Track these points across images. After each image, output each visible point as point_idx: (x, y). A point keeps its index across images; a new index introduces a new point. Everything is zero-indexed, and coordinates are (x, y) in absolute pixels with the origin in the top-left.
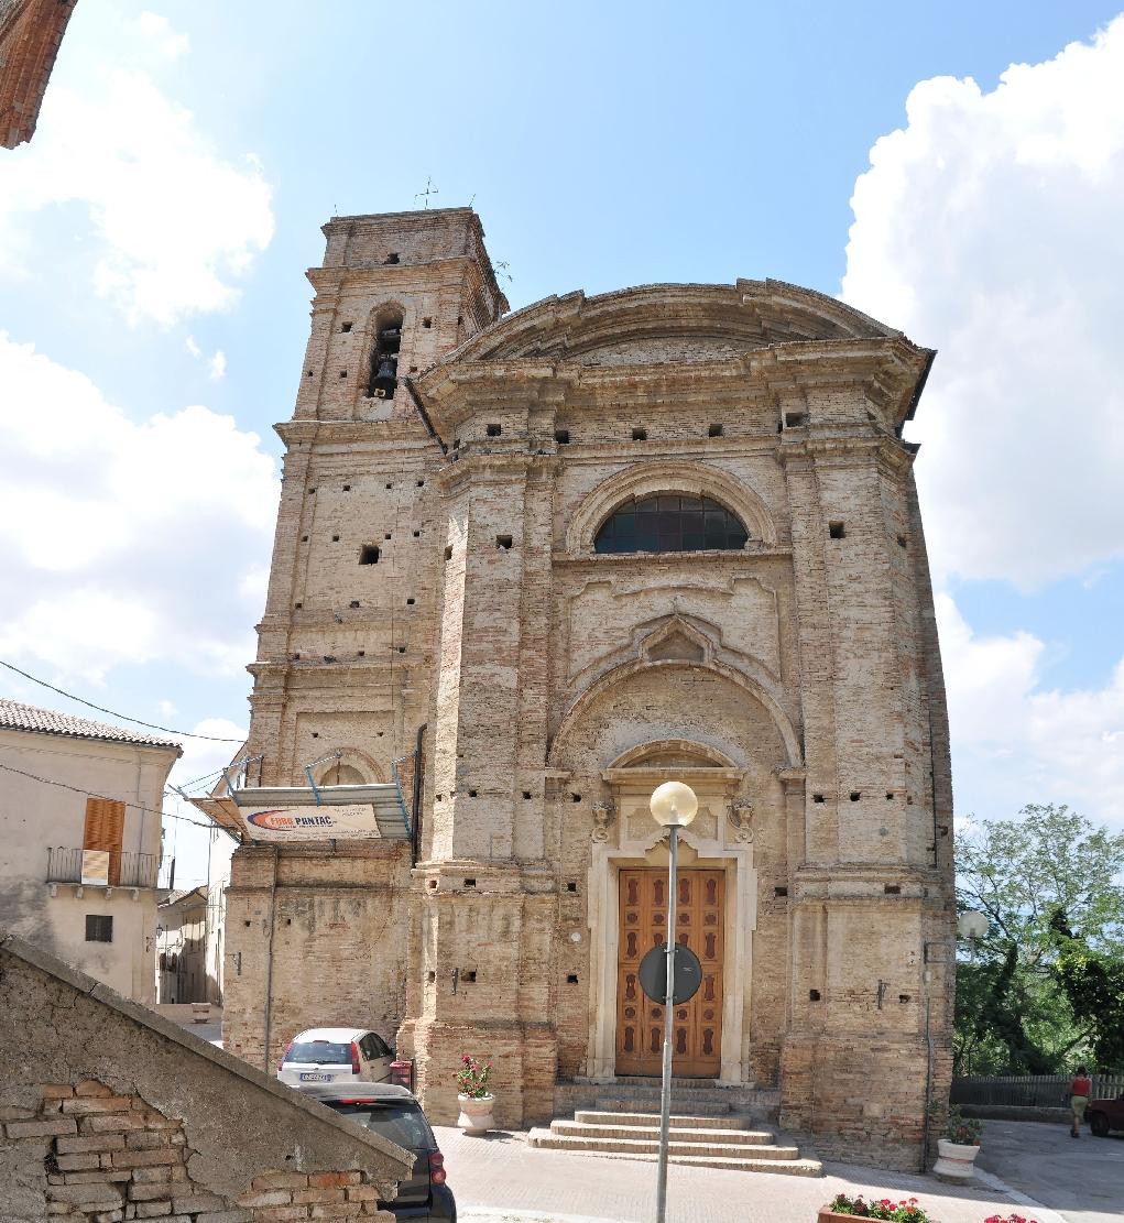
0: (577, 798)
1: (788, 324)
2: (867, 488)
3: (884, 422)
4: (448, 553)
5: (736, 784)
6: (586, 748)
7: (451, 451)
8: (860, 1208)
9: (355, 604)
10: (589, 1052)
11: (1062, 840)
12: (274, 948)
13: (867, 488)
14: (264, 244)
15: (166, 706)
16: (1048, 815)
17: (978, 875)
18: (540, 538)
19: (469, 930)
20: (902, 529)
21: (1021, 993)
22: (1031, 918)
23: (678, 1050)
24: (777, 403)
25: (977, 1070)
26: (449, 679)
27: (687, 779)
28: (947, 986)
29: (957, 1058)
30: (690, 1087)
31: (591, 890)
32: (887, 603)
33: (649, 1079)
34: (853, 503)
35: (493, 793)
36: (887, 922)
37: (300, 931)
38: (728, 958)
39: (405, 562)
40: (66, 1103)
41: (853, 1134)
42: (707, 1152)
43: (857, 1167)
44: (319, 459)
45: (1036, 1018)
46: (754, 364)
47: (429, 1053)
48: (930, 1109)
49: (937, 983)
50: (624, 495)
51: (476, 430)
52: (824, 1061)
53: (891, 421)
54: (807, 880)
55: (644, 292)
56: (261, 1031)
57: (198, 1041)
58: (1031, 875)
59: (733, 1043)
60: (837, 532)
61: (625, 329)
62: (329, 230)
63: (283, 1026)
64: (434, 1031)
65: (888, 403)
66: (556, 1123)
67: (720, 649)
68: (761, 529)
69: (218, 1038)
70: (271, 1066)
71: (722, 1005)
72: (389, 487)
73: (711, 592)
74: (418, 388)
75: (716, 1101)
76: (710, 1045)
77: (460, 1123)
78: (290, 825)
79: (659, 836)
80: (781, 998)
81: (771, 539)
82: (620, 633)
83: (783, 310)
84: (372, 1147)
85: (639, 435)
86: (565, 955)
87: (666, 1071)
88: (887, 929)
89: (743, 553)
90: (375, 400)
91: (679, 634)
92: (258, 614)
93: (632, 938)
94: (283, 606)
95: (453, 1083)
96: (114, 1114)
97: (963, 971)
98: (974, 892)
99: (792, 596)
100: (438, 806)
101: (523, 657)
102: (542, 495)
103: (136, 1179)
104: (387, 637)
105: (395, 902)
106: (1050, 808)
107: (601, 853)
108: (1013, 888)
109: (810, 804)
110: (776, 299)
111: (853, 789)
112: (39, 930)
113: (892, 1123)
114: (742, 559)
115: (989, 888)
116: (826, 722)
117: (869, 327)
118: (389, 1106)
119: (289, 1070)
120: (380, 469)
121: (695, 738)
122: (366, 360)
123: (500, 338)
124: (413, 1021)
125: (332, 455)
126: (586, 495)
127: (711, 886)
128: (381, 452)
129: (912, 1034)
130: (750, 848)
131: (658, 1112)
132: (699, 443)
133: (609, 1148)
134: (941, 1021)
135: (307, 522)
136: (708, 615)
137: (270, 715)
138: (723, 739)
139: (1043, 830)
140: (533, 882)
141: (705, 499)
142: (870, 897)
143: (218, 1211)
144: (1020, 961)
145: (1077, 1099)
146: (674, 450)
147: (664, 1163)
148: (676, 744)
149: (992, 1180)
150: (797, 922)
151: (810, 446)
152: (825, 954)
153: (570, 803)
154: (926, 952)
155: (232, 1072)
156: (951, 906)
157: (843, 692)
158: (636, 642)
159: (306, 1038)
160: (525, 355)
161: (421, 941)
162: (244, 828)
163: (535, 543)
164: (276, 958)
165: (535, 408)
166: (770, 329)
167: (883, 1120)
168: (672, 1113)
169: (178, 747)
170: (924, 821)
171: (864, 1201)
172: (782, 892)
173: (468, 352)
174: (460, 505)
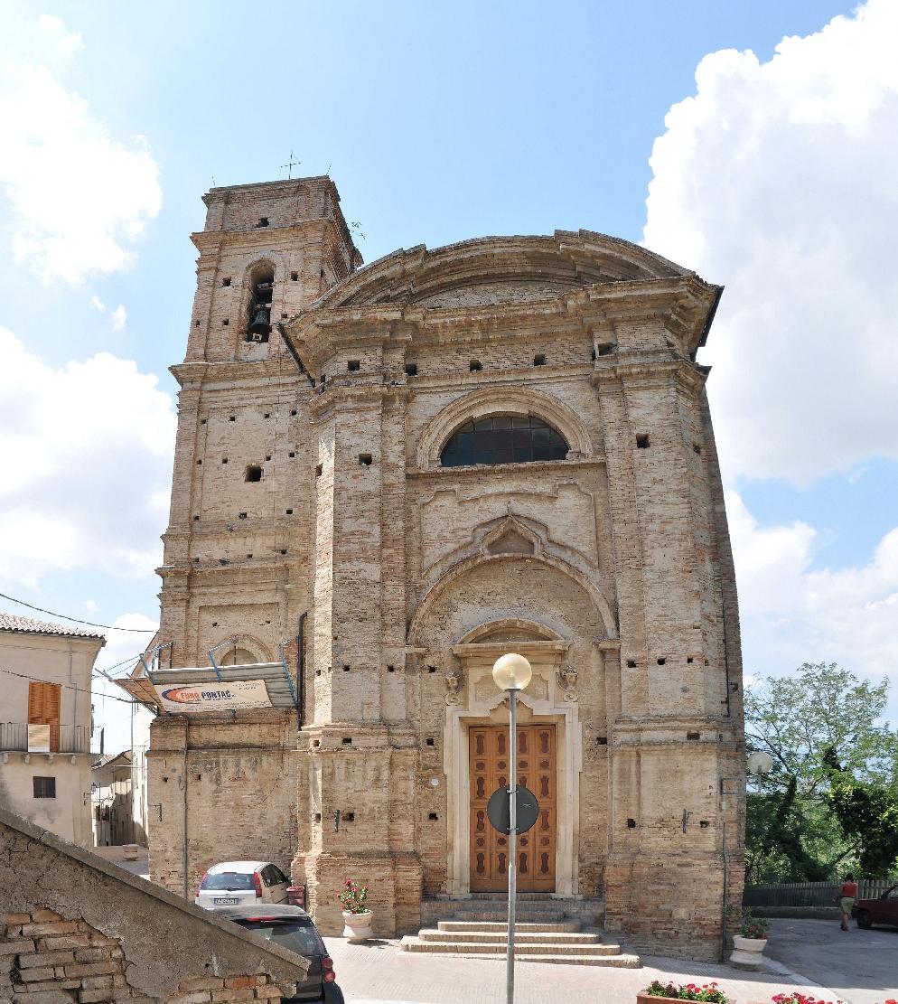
0: (432, 670)
1: (598, 268)
3: (680, 349)
4: (319, 471)
5: (562, 654)
6: (439, 629)
7: (318, 385)
8: (671, 992)
9: (244, 516)
10: (448, 874)
11: (833, 691)
12: (188, 799)
14: (154, 212)
15: (90, 604)
19: (348, 776)
20: (698, 439)
21: (799, 816)
24: (591, 336)
25: (764, 878)
26: (323, 576)
29: (748, 870)
32: (686, 500)
35: (363, 667)
38: (560, 796)
41: (664, 934)
42: (546, 951)
43: (668, 960)
44: (208, 395)
45: (812, 836)
46: (570, 303)
47: (318, 879)
48: (727, 911)
49: (732, 810)
50: (465, 417)
51: (340, 365)
52: (639, 876)
53: (686, 348)
54: (622, 730)
57: (129, 875)
58: (807, 721)
59: (565, 864)
60: (643, 442)
62: (208, 199)
63: (198, 861)
65: (684, 333)
66: (423, 932)
68: (581, 443)
72: (267, 416)
73: (539, 496)
74: (289, 332)
75: (552, 910)
76: (547, 866)
77: (345, 934)
78: (196, 699)
79: (500, 698)
81: (588, 450)
83: (594, 256)
85: (476, 366)
87: (512, 889)
91: (513, 532)
92: (163, 526)
93: (480, 782)
94: (184, 518)
96: (65, 935)
97: (752, 800)
99: (606, 497)
100: (318, 679)
101: (384, 556)
102: (396, 419)
106: (822, 666)
108: (792, 731)
109: (625, 668)
111: (660, 655)
115: (773, 733)
116: (636, 601)
118: (289, 922)
120: (260, 401)
121: (529, 618)
122: (244, 309)
123: (356, 288)
126: (432, 418)
127: (544, 738)
129: (709, 852)
130: (576, 706)
131: (506, 921)
132: (526, 371)
133: (467, 950)
134: (734, 841)
135: (201, 448)
136: (537, 517)
137: (177, 609)
138: (552, 617)
139: (816, 684)
140: (399, 739)
141: (532, 418)
142: (675, 742)
144: (798, 791)
150: (616, 766)
151: (619, 371)
152: (639, 790)
153: (426, 674)
156: (741, 748)
158: (478, 540)
159: (217, 870)
160: (378, 301)
161: (307, 790)
162: (159, 702)
163: (392, 459)
165: (387, 347)
166: (584, 273)
169: (102, 637)
170: (718, 679)
173: (329, 301)
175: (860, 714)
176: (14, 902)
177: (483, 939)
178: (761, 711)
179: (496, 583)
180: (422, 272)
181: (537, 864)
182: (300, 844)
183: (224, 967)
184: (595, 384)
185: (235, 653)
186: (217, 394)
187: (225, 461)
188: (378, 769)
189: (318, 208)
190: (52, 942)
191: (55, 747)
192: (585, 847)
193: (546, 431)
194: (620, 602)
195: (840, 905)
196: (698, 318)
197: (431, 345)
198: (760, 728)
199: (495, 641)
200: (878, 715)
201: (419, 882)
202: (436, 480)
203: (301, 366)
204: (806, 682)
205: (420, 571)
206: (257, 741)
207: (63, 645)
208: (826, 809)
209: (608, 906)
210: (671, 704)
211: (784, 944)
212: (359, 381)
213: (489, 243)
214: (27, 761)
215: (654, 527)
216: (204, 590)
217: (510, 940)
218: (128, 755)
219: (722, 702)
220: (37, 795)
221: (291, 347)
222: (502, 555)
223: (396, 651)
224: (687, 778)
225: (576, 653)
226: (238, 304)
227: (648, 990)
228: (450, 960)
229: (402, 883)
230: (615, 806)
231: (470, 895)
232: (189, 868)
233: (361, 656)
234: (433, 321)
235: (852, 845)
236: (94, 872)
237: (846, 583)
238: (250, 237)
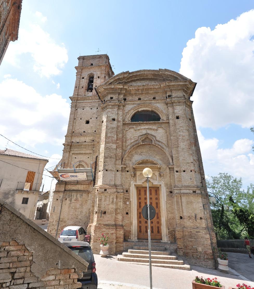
1: (168, 78)
2: (183, 109)
3: (186, 96)
4: (103, 122)
5: (160, 168)
7: (103, 102)
9: (84, 132)
11: (228, 181)
12: (62, 206)
13: (183, 109)
14: (66, 62)
15: (46, 152)
16: (224, 175)
17: (212, 188)
18: (120, 119)
19: (105, 201)
20: (190, 117)
21: (227, 217)
22: (225, 199)
23: (152, 232)
24: (166, 93)
25: (221, 238)
26: (102, 146)
27: (150, 167)
28: (210, 215)
29: (216, 234)
30: (155, 243)
31: (131, 192)
32: (188, 131)
33: (145, 240)
34: (180, 112)
35: (111, 170)
36: (194, 199)
37: (68, 201)
39: (94, 124)
40: (6, 248)
44: (78, 104)
45: (232, 223)
46: (162, 85)
47: (94, 233)
48: (213, 249)
49: (208, 215)
50: (137, 111)
51: (108, 98)
52: (186, 235)
53: (188, 96)
54: (176, 189)
55: (141, 71)
56: (57, 227)
57: (41, 229)
58: (223, 188)
59: (164, 230)
60: (178, 118)
61: (137, 78)
62: (79, 59)
63: (62, 225)
64: (96, 227)
66: (124, 253)
67: (156, 141)
68: (163, 118)
69: (46, 229)
70: (57, 236)
71: (160, 220)
72: (91, 109)
73: (154, 129)
74: (97, 90)
75: (162, 247)
76: (159, 231)
78: (68, 177)
79: (145, 179)
80: (174, 218)
82: (136, 138)
83: (168, 75)
84: (78, 261)
85: (140, 99)
86: (125, 207)
87: (149, 238)
88: (195, 201)
89: (160, 122)
90: (89, 92)
91: (148, 138)
92: (65, 133)
95: (99, 241)
96: (17, 250)
97: (213, 211)
98: (212, 192)
99: (169, 130)
100: (99, 173)
102: (121, 110)
103: (17, 271)
104: (91, 138)
105: (89, 194)
106: (224, 174)
107: (133, 184)
108: (220, 191)
109: (175, 173)
110: (166, 73)
111: (184, 170)
112: (12, 201)
113: (205, 253)
114: (159, 123)
115: (215, 192)
117: (184, 78)
118: (84, 248)
119: (61, 238)
120: (90, 105)
121: (151, 159)
122: (87, 84)
124: (91, 224)
125: (81, 103)
126: (129, 111)
127: (156, 191)
128: (90, 102)
129: (205, 228)
131: (148, 250)
132: (151, 101)
133: (137, 261)
134: (210, 224)
137: (67, 154)
138: (157, 159)
139: (224, 178)
141: (152, 111)
142: (190, 193)
143: (36, 282)
144: (225, 209)
145: (248, 246)
146: (146, 102)
147: (151, 266)
148: (147, 160)
149: (233, 271)
150: (175, 200)
151: (172, 101)
152: (182, 207)
154: (204, 207)
155: (48, 238)
156: (207, 196)
157: (180, 149)
158: (139, 139)
160: (118, 84)
161: (94, 204)
162: (59, 178)
163: (120, 120)
164: (62, 208)
165: (119, 94)
167: (203, 252)
168: (152, 250)
169: (48, 160)
170: (199, 176)
171: (203, 279)
172: (171, 192)
173: (106, 83)
174: (104, 113)
175: (236, 187)
176: (6, 237)
177: (142, 257)
178: (211, 185)
179: (145, 150)
180: (128, 77)
181: (156, 230)
182: (90, 221)
183: (63, 265)
184: (167, 104)
185: (80, 165)
186: (80, 104)
187: (81, 119)
188: (113, 199)
189: (104, 62)
190: (13, 253)
191: (30, 189)
192: (169, 225)
193: (155, 114)
194: (173, 155)
195: (246, 248)
196: (191, 90)
197: (129, 94)
198: (211, 190)
199: (143, 165)
200: (241, 187)
201: (122, 235)
202: (130, 125)
203: (100, 98)
204: (221, 178)
205: (125, 146)
206: (82, 189)
207: (38, 162)
208: (233, 215)
209: (178, 246)
210: (188, 183)
211: (234, 262)
212: (112, 102)
213: (144, 71)
214: (23, 193)
215: (180, 137)
216: (74, 149)
217: (150, 257)
218: (49, 192)
219: (200, 183)
220: (22, 203)
221: (97, 93)
222: (145, 143)
223: (119, 166)
224: (194, 204)
225: (163, 169)
226: (86, 83)
227: (195, 280)
228: (132, 265)
229: (118, 235)
230: (176, 212)
231: (137, 240)
232: (59, 228)
233: (109, 167)
234: (130, 88)
235: (244, 227)
236: (32, 228)
237: (227, 152)
238: (89, 68)
